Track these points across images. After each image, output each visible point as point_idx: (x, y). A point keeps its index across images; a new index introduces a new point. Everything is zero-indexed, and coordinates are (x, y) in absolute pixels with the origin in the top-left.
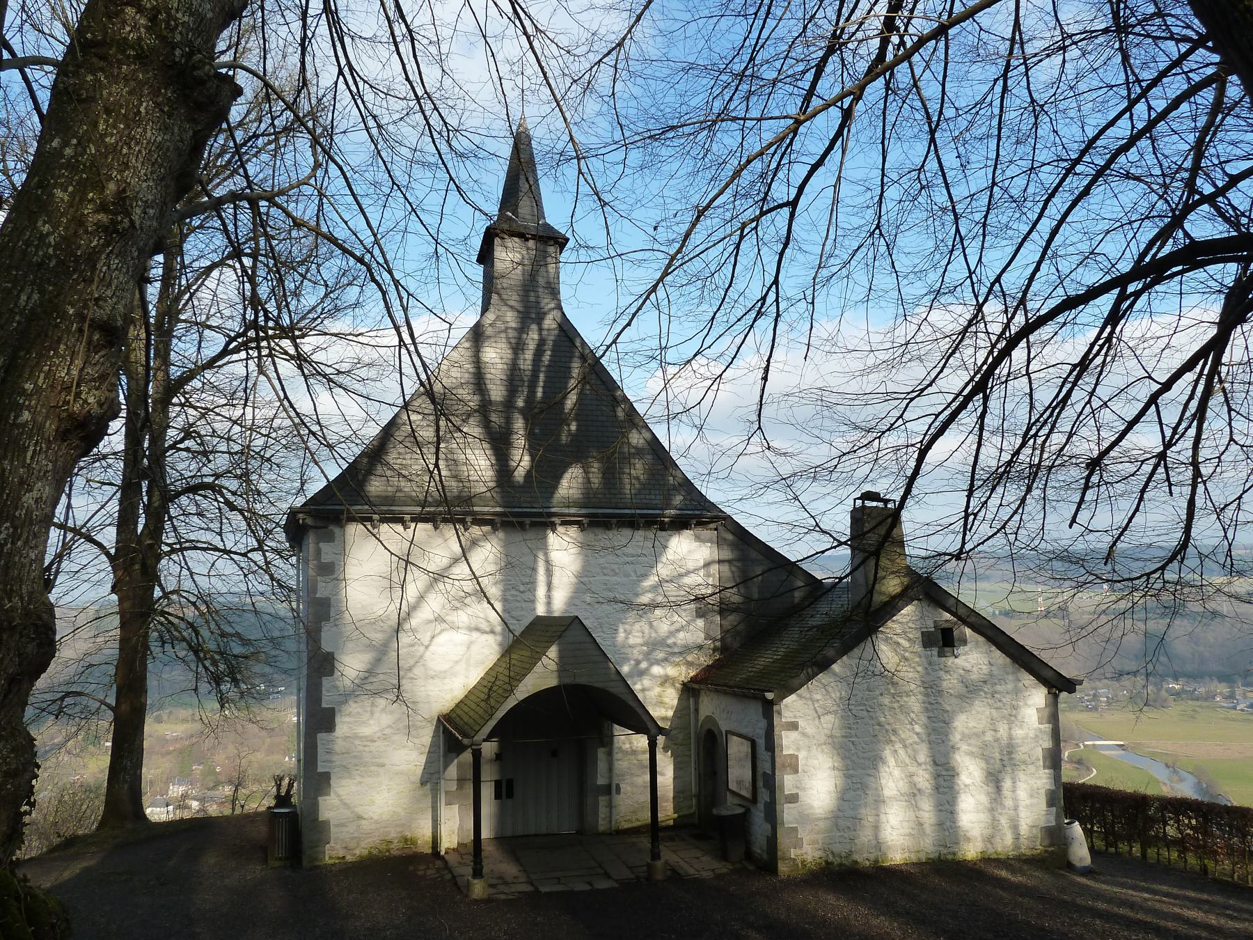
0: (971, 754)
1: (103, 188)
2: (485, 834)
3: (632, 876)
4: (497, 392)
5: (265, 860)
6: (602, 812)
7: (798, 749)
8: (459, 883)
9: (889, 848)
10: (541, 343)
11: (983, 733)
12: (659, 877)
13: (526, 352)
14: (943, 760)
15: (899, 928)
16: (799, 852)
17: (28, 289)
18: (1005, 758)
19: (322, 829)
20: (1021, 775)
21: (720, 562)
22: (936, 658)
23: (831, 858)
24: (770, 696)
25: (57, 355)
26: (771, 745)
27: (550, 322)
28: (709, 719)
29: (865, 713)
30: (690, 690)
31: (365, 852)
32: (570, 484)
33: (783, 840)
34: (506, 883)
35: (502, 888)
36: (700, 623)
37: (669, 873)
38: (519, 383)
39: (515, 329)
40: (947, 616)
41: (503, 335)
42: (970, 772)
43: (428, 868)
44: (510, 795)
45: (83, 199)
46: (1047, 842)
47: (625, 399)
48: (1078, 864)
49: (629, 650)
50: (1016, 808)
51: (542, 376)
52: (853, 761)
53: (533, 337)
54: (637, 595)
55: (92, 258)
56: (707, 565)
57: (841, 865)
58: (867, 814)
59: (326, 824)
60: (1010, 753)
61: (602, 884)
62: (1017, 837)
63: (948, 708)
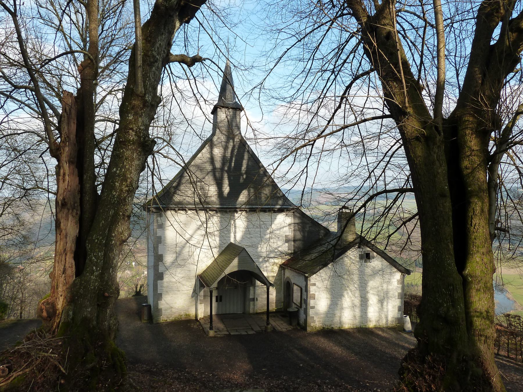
0: (373, 294)
1: (127, 181)
2: (213, 313)
3: (260, 330)
4: (218, 165)
5: (141, 319)
6: (252, 306)
7: (315, 292)
8: (205, 331)
9: (344, 323)
10: (234, 146)
11: (378, 287)
12: (269, 331)
13: (228, 150)
14: (364, 296)
15: (341, 351)
16: (314, 324)
17: (112, 210)
18: (385, 295)
19: (159, 311)
20: (390, 301)
21: (294, 223)
22: (363, 263)
23: (324, 326)
24: (307, 275)
25: (118, 226)
26: (306, 291)
27: (237, 139)
28: (288, 278)
29: (338, 281)
30: (282, 267)
31: (174, 319)
32: (243, 197)
33: (309, 320)
34: (220, 331)
35: (219, 333)
36: (287, 244)
37: (272, 329)
38: (226, 161)
39: (224, 142)
40: (369, 249)
41: (220, 144)
42: (373, 300)
43: (194, 325)
44: (221, 301)
45: (122, 184)
46: (397, 322)
47: (263, 166)
48: (407, 330)
49: (262, 254)
50: (387, 312)
51: (234, 159)
52: (333, 296)
53: (231, 144)
54: (265, 235)
55: (125, 199)
56: (289, 225)
57: (328, 328)
58: (338, 313)
59: (161, 309)
60: (387, 294)
61: (251, 332)
62: (387, 321)
63: (366, 279)
